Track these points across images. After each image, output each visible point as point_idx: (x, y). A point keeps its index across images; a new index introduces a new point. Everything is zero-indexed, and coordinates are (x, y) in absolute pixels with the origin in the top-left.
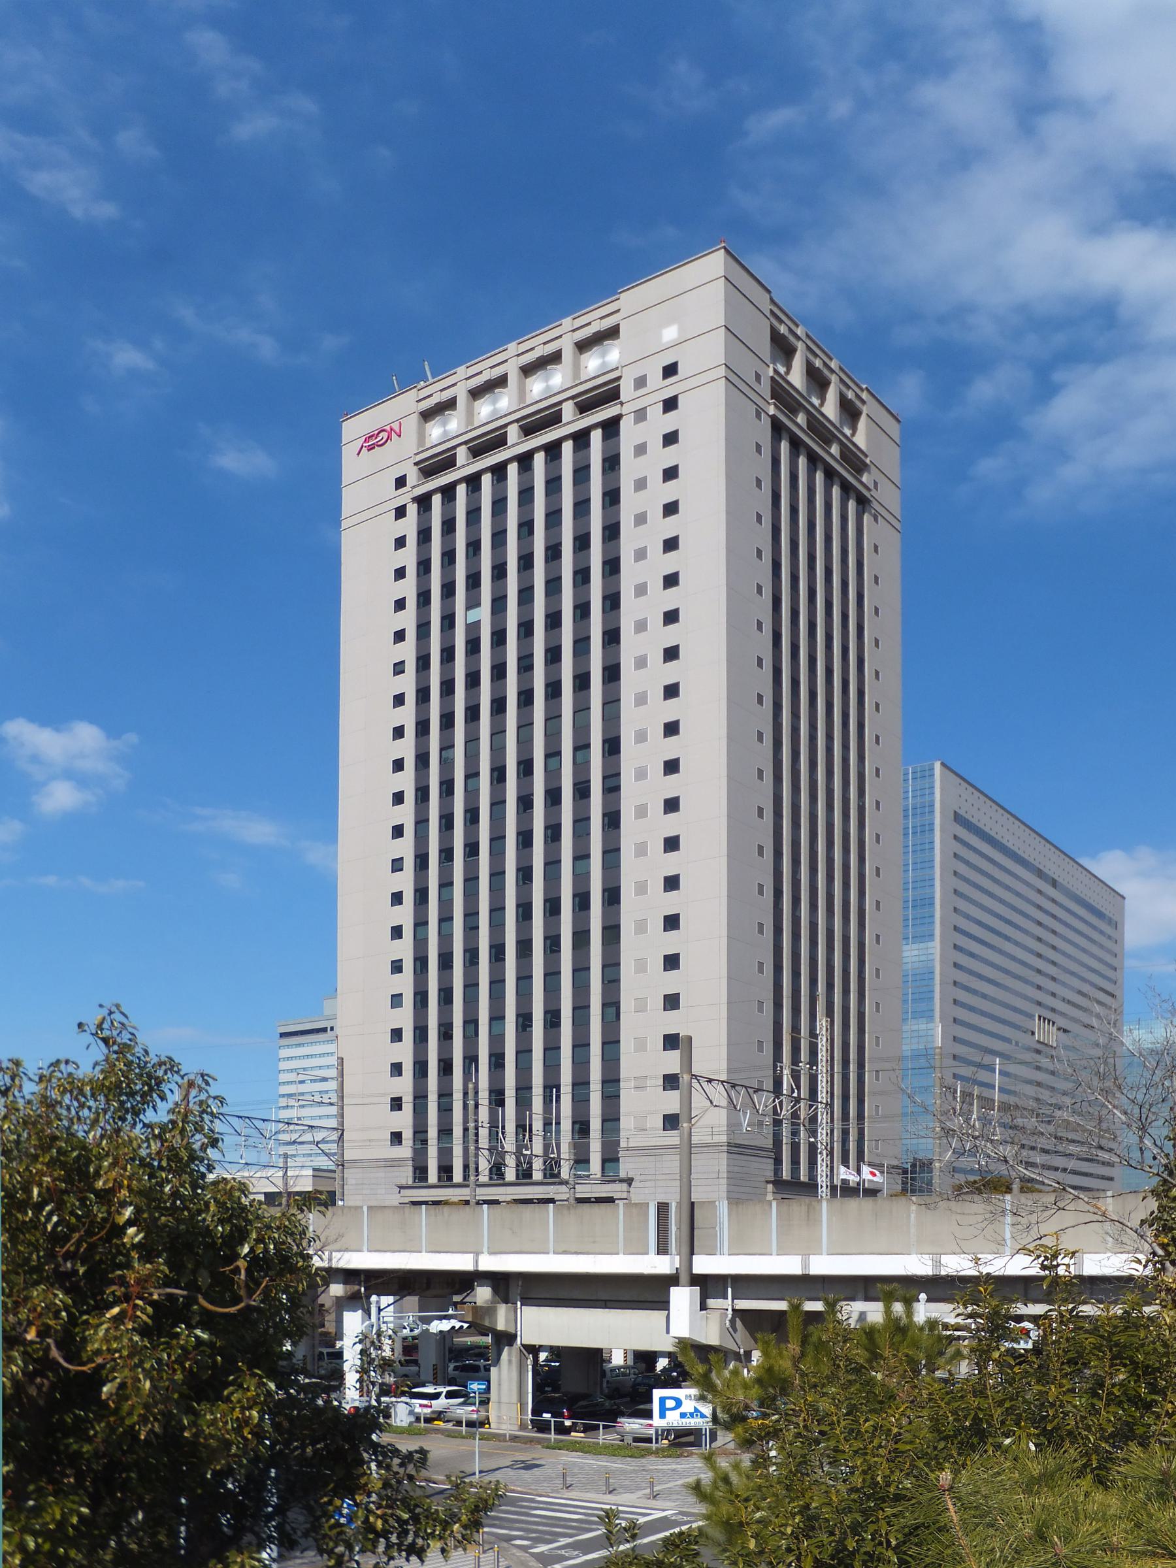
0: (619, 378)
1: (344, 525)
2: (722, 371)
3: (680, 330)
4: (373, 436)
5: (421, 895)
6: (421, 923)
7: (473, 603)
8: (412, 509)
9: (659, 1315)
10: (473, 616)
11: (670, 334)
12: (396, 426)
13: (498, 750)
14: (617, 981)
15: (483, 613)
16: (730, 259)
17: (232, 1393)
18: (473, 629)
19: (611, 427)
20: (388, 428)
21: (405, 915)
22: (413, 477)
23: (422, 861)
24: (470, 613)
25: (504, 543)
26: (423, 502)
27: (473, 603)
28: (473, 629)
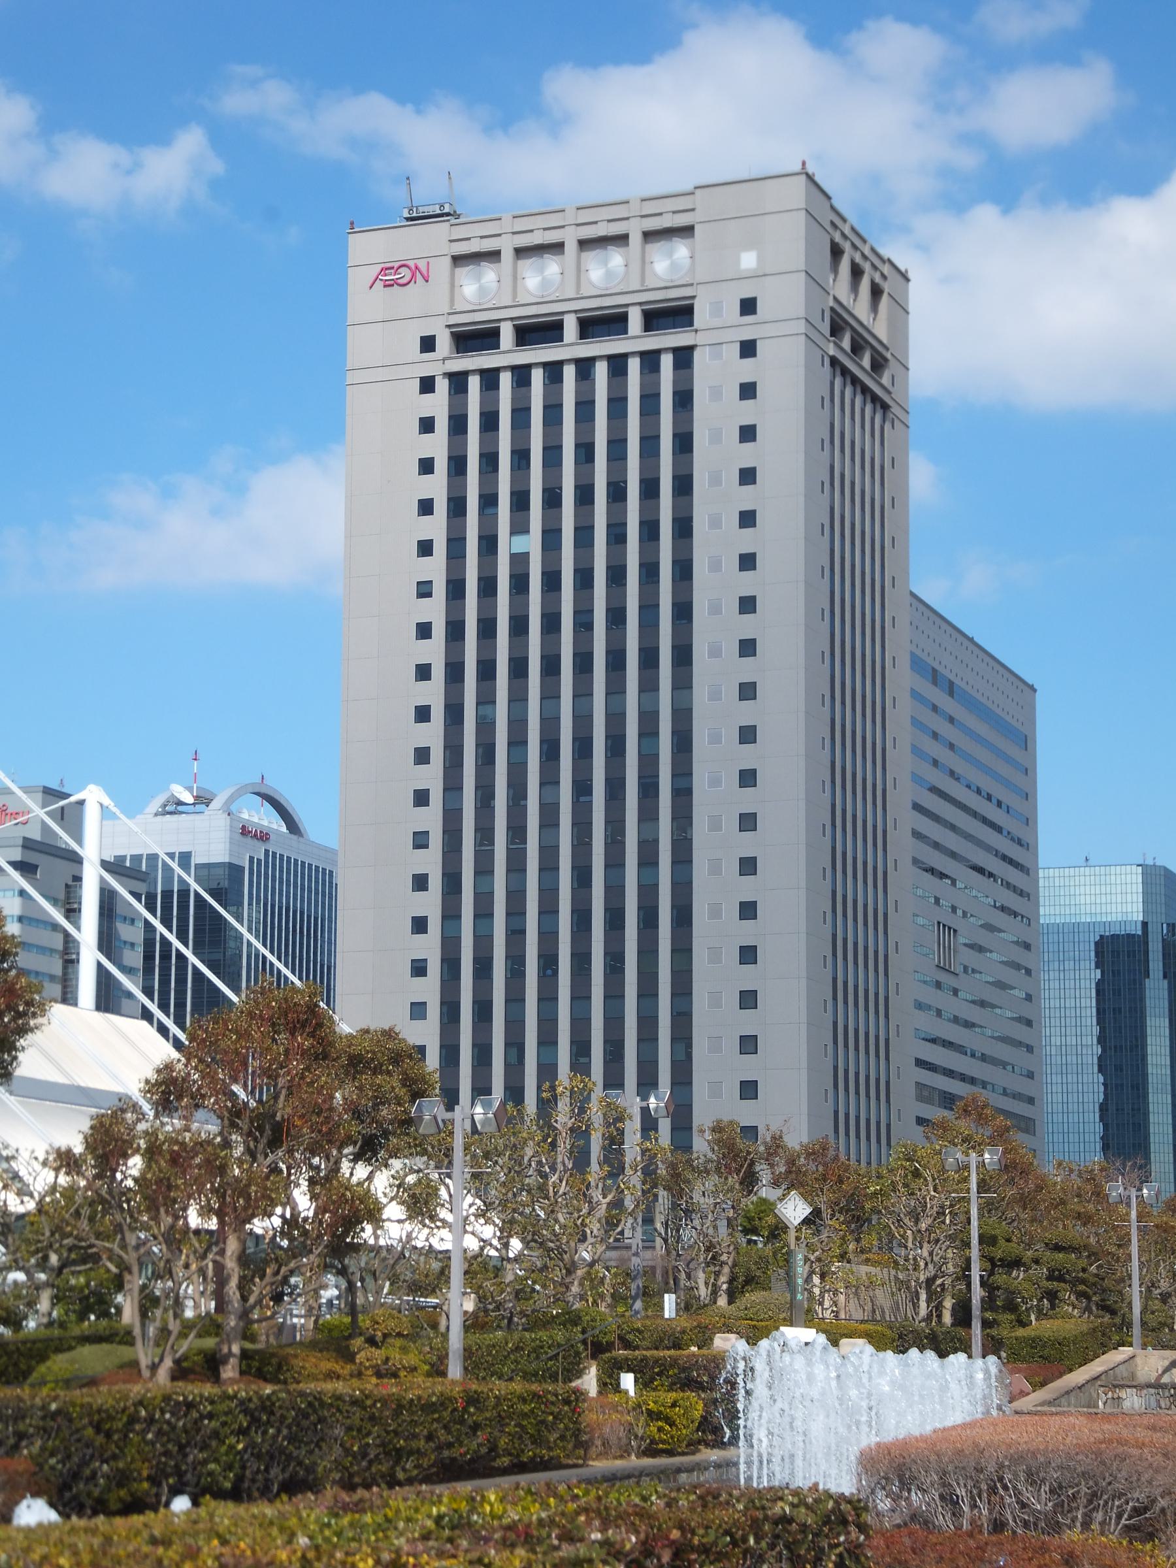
0: (694, 297)
1: (351, 378)
2: (801, 327)
3: (760, 259)
4: (392, 268)
5: (454, 713)
6: (451, 914)
7: (520, 527)
8: (442, 385)
9: (758, 343)
10: (521, 544)
11: (749, 260)
12: (422, 265)
13: (550, 694)
14: (689, 792)
15: (532, 543)
16: (810, 184)
17: (186, 1290)
18: (520, 561)
19: (684, 357)
20: (411, 264)
21: (430, 903)
22: (444, 343)
23: (456, 589)
24: (515, 539)
25: (559, 464)
26: (458, 381)
27: (520, 527)
28: (520, 561)
